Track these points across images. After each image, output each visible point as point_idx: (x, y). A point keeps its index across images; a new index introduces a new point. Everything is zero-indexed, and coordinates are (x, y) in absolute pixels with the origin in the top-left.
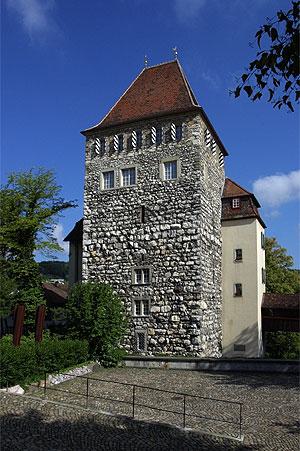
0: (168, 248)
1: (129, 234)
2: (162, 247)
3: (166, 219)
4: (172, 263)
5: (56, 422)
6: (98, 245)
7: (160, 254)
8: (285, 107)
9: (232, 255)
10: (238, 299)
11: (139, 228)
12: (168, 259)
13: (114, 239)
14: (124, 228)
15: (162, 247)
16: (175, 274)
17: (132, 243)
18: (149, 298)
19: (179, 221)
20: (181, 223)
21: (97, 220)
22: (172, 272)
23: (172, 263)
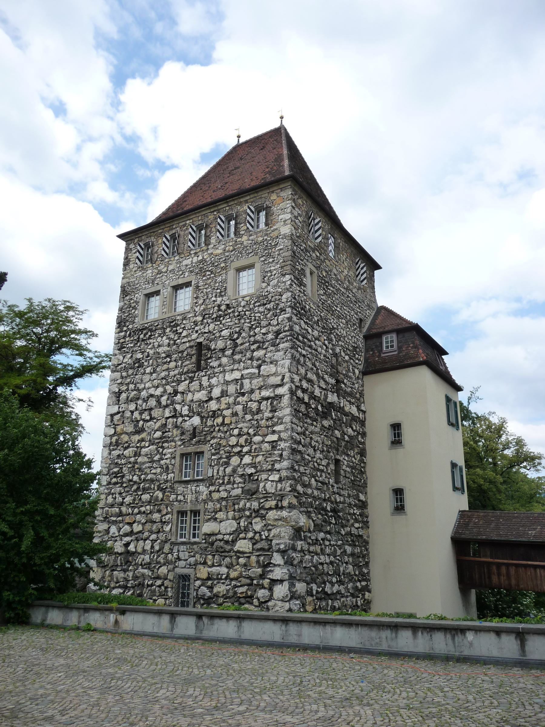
0: (235, 414)
1: (176, 393)
2: (225, 412)
3: (234, 362)
4: (242, 440)
5: (489, 499)
6: (128, 414)
7: (223, 424)
8: (478, 400)
9: (386, 435)
10: (400, 518)
11: (192, 380)
12: (236, 432)
13: (152, 402)
14: (168, 384)
15: (227, 413)
16: (247, 459)
17: (178, 407)
18: (200, 507)
19: (255, 363)
20: (259, 367)
21: (130, 372)
22: (240, 455)
23: (242, 440)
